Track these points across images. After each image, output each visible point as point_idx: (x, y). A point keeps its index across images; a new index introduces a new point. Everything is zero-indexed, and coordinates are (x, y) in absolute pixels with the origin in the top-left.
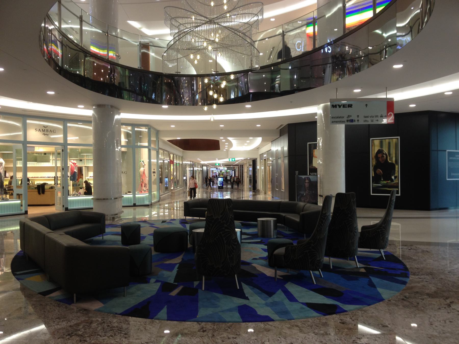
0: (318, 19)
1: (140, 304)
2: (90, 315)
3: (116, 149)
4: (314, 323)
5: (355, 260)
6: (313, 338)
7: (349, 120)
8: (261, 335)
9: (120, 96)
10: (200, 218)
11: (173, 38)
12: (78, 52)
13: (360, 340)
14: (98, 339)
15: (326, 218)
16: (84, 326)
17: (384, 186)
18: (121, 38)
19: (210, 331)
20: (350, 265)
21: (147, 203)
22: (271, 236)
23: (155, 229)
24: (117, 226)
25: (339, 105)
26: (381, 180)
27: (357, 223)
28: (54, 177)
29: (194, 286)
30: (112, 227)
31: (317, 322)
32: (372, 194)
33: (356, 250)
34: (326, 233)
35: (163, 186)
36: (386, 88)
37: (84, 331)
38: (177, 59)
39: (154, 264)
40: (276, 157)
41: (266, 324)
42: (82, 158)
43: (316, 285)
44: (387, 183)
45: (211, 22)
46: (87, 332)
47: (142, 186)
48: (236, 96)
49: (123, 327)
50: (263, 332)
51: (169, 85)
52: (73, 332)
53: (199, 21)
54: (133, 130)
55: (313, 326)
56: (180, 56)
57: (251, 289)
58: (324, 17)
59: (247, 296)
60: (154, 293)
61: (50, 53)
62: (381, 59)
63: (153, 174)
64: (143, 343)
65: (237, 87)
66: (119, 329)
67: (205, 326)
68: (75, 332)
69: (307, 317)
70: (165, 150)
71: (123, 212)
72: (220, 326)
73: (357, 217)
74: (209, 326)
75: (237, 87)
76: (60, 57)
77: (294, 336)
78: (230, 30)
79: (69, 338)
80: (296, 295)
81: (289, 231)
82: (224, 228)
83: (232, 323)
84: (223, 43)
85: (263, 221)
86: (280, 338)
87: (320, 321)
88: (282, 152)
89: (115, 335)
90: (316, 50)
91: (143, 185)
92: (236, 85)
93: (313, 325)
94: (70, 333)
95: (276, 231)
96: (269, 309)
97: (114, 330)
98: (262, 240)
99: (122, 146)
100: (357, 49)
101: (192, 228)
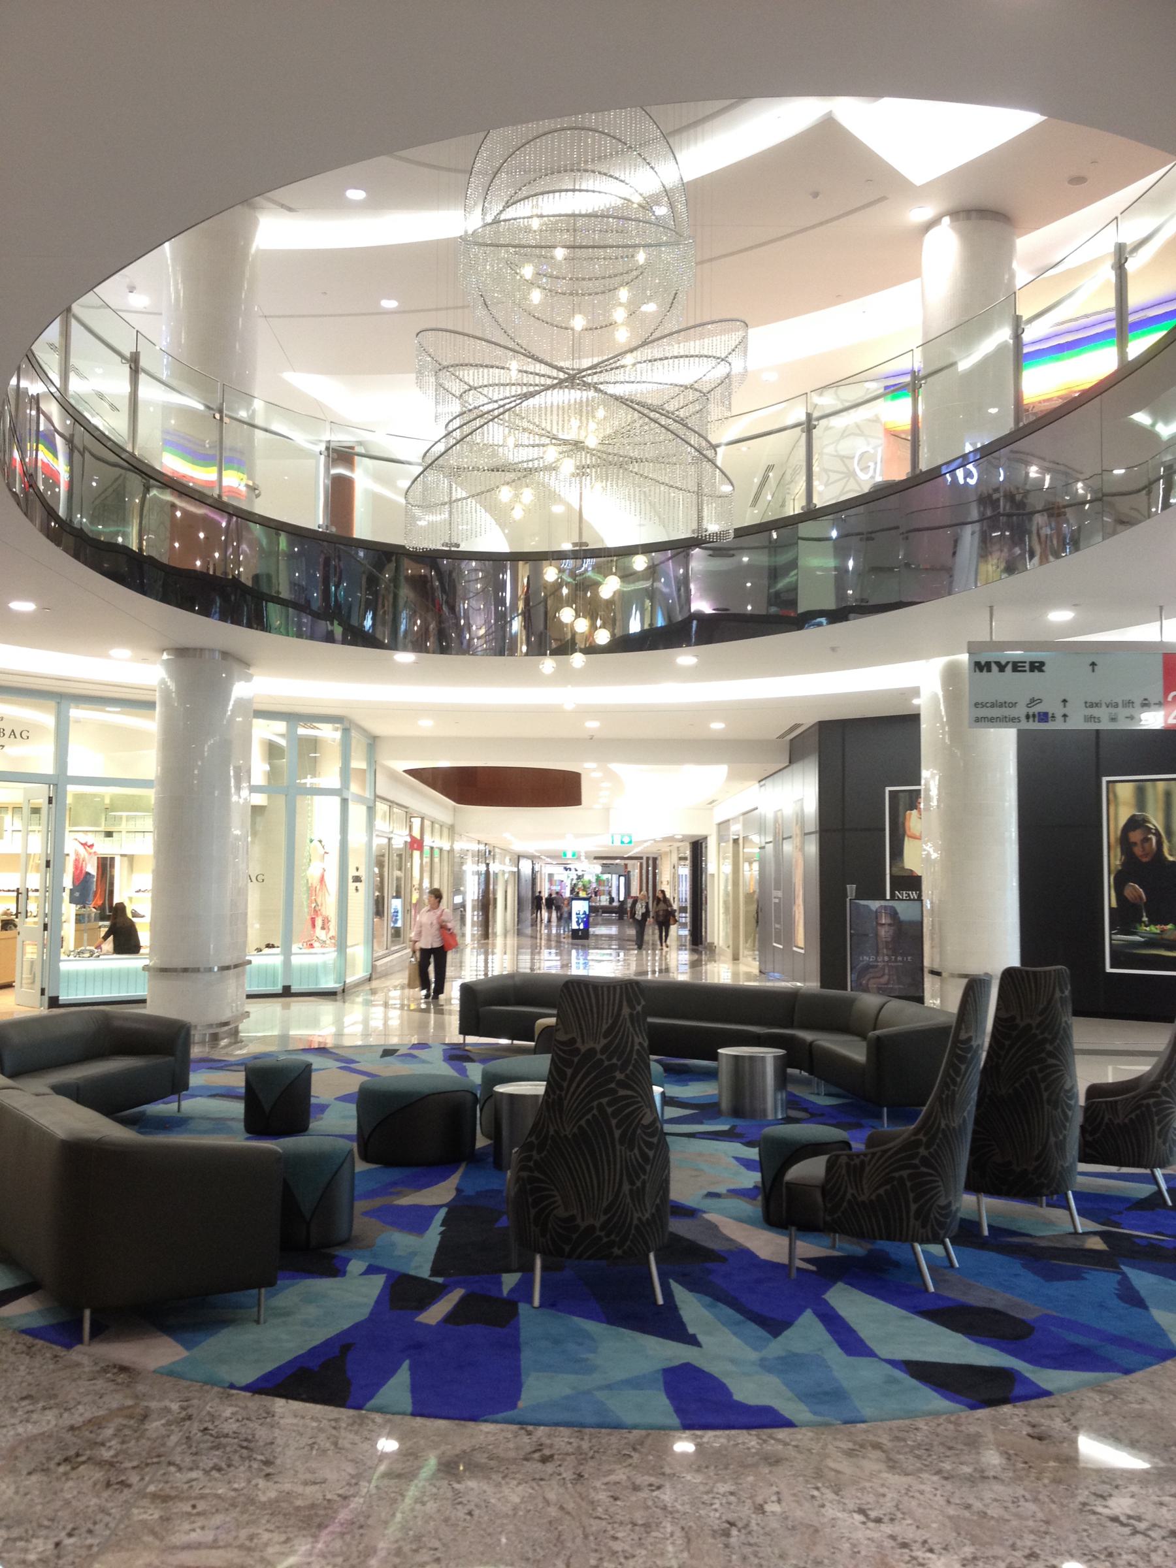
0: (925, 377)
1: (313, 1352)
2: (141, 1388)
3: (234, 798)
4: (938, 1435)
5: (1069, 1208)
6: (938, 1493)
7: (1034, 716)
8: (751, 1479)
9: (258, 622)
10: (515, 1042)
11: (444, 433)
12: (123, 471)
13: (1104, 1503)
14: (171, 1479)
15: (969, 1055)
16: (120, 1430)
17: (1151, 943)
18: (266, 430)
19: (568, 1458)
20: (1049, 1223)
21: (329, 984)
22: (764, 1111)
23: (365, 1078)
24: (226, 1066)
25: (998, 664)
26: (1141, 922)
27: (1076, 1076)
28: (15, 889)
29: (501, 1290)
30: (211, 1068)
31: (946, 1433)
32: (1109, 970)
33: (1071, 1169)
34: (969, 1111)
35: (386, 926)
36: (1161, 608)
37: (119, 1447)
38: (451, 502)
39: (360, 1206)
40: (775, 837)
41: (764, 1437)
42: (114, 825)
43: (936, 1295)
44: (1163, 931)
45: (573, 380)
46: (130, 1452)
47: (314, 926)
48: (646, 627)
49: (257, 1437)
50: (755, 1465)
51: (420, 585)
52: (81, 1452)
53: (531, 379)
54: (290, 735)
55: (935, 1448)
56: (459, 493)
57: (707, 1306)
58: (953, 368)
59: (691, 1330)
60: (363, 1313)
61: (30, 477)
62: (1149, 509)
63: (352, 886)
64: (329, 1496)
65: (651, 594)
66: (245, 1444)
67: (548, 1442)
68: (88, 1452)
69: (912, 1415)
70: (397, 804)
71: (248, 1016)
72: (603, 1441)
73: (1073, 1052)
74: (562, 1440)
75: (651, 594)
76: (63, 490)
77: (868, 1485)
78: (634, 409)
79: (65, 1474)
80: (866, 1332)
81: (828, 1095)
82: (613, 1085)
83: (643, 1432)
84: (610, 451)
85: (736, 1057)
86: (817, 1489)
87: (957, 1431)
88: (797, 816)
89: (229, 1466)
90: (920, 479)
91: (319, 923)
92: (646, 589)
93: (935, 1443)
94: (72, 1453)
95: (781, 1096)
96: (774, 1381)
97: (225, 1447)
98: (733, 1127)
99: (254, 789)
100: (1066, 475)
101: (492, 1079)
